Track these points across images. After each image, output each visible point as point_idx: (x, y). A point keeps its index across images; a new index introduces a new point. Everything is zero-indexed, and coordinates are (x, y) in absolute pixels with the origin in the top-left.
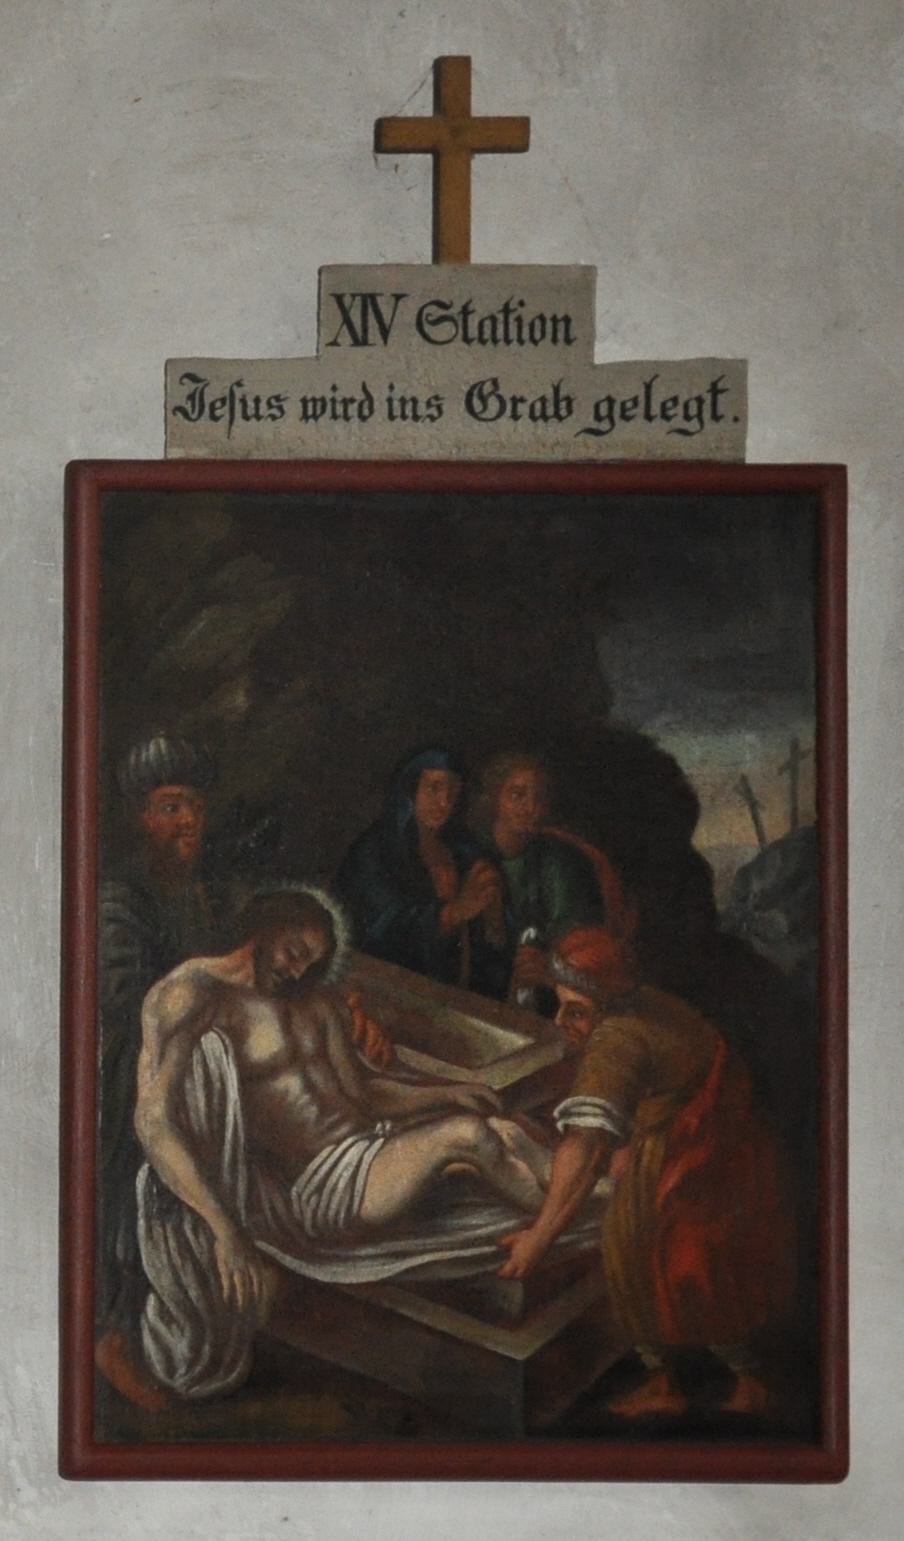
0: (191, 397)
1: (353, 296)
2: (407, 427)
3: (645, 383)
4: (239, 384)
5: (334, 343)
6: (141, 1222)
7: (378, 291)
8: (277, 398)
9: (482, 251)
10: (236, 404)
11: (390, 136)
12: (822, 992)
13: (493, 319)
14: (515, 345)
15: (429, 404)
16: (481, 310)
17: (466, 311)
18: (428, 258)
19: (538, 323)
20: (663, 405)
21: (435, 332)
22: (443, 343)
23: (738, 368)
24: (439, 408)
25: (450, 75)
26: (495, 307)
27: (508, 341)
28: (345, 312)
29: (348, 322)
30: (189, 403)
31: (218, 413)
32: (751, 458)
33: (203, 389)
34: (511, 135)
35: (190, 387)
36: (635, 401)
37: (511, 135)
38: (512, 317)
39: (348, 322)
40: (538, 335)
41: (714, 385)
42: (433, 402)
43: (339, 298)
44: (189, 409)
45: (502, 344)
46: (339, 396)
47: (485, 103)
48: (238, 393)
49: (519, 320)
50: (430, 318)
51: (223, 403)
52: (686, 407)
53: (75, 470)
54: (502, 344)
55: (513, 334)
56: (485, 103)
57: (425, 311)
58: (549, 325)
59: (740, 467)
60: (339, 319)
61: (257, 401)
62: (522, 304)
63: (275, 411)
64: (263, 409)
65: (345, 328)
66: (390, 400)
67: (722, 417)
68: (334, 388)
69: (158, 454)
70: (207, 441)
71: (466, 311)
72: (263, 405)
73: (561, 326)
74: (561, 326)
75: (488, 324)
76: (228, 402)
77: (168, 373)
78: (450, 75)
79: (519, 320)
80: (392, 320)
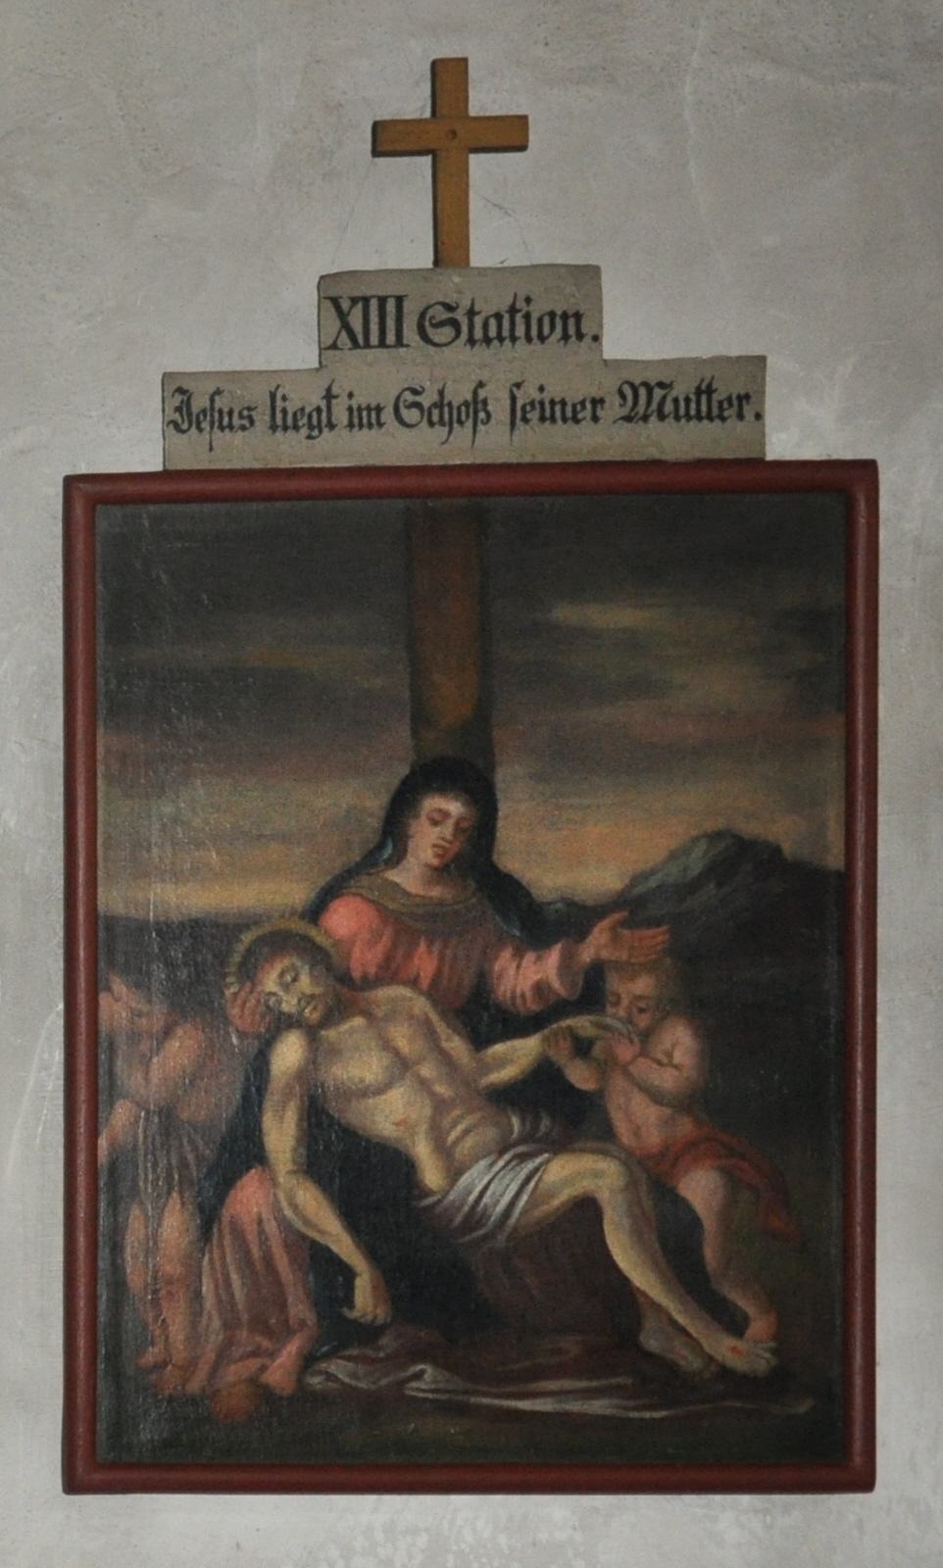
0: (178, 409)
1: (354, 301)
2: (363, 436)
3: (218, 389)
4: (481, 385)
5: (334, 346)
6: (524, 1405)
7: (403, 294)
8: (249, 409)
9: (481, 255)
10: (222, 419)
11: (388, 140)
12: (847, 1057)
13: (498, 317)
14: (521, 343)
15: (241, 416)
16: (486, 309)
17: (471, 313)
18: (426, 260)
19: (546, 321)
20: (720, 403)
21: (438, 335)
22: (450, 343)
23: (167, 377)
24: (252, 422)
25: (449, 77)
26: (503, 306)
27: (514, 339)
28: (342, 315)
29: (346, 326)
30: (177, 414)
31: (580, 416)
32: (771, 455)
33: (189, 399)
34: (509, 135)
35: (179, 398)
36: (204, 411)
37: (509, 135)
38: (519, 318)
39: (346, 326)
40: (546, 330)
41: (329, 390)
42: (245, 413)
43: (335, 302)
44: (180, 421)
45: (507, 342)
46: (546, 397)
47: (484, 100)
48: (482, 394)
49: (527, 317)
50: (434, 322)
51: (731, 405)
52: (310, 416)
53: (71, 483)
54: (507, 342)
55: (520, 331)
56: (484, 100)
57: (430, 313)
58: (534, 332)
59: (759, 463)
60: (338, 324)
61: (230, 413)
62: (528, 300)
63: (245, 422)
64: (236, 421)
65: (344, 334)
66: (350, 409)
67: (385, 423)
68: (541, 389)
69: (155, 465)
70: (196, 452)
71: (471, 313)
72: (236, 415)
73: (571, 322)
74: (571, 322)
75: (493, 322)
76: (209, 414)
77: (165, 387)
78: (449, 77)
79: (527, 317)
80: (339, 333)
